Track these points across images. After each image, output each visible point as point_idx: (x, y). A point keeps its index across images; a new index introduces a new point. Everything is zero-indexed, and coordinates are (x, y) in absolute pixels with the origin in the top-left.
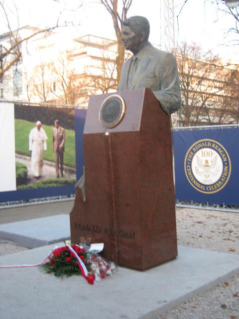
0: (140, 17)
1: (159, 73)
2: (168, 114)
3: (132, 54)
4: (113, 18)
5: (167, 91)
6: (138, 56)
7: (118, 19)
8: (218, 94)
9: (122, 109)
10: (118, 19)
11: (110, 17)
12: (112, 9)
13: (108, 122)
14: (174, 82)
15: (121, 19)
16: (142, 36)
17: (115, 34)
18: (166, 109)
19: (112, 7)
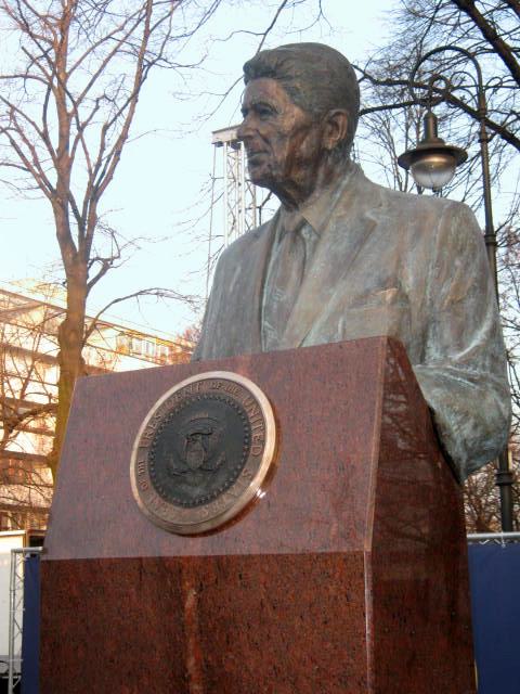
0: (334, 50)
1: (421, 284)
2: (462, 473)
3: (275, 203)
4: (55, 212)
5: (461, 364)
6: (312, 213)
7: (70, 210)
8: (16, 627)
9: (263, 442)
10: (70, 210)
11: (46, 207)
12: (55, 187)
13: (187, 506)
14: (486, 327)
15: (81, 213)
16: (335, 125)
17: (61, 257)
18: (456, 451)
19: (53, 177)
